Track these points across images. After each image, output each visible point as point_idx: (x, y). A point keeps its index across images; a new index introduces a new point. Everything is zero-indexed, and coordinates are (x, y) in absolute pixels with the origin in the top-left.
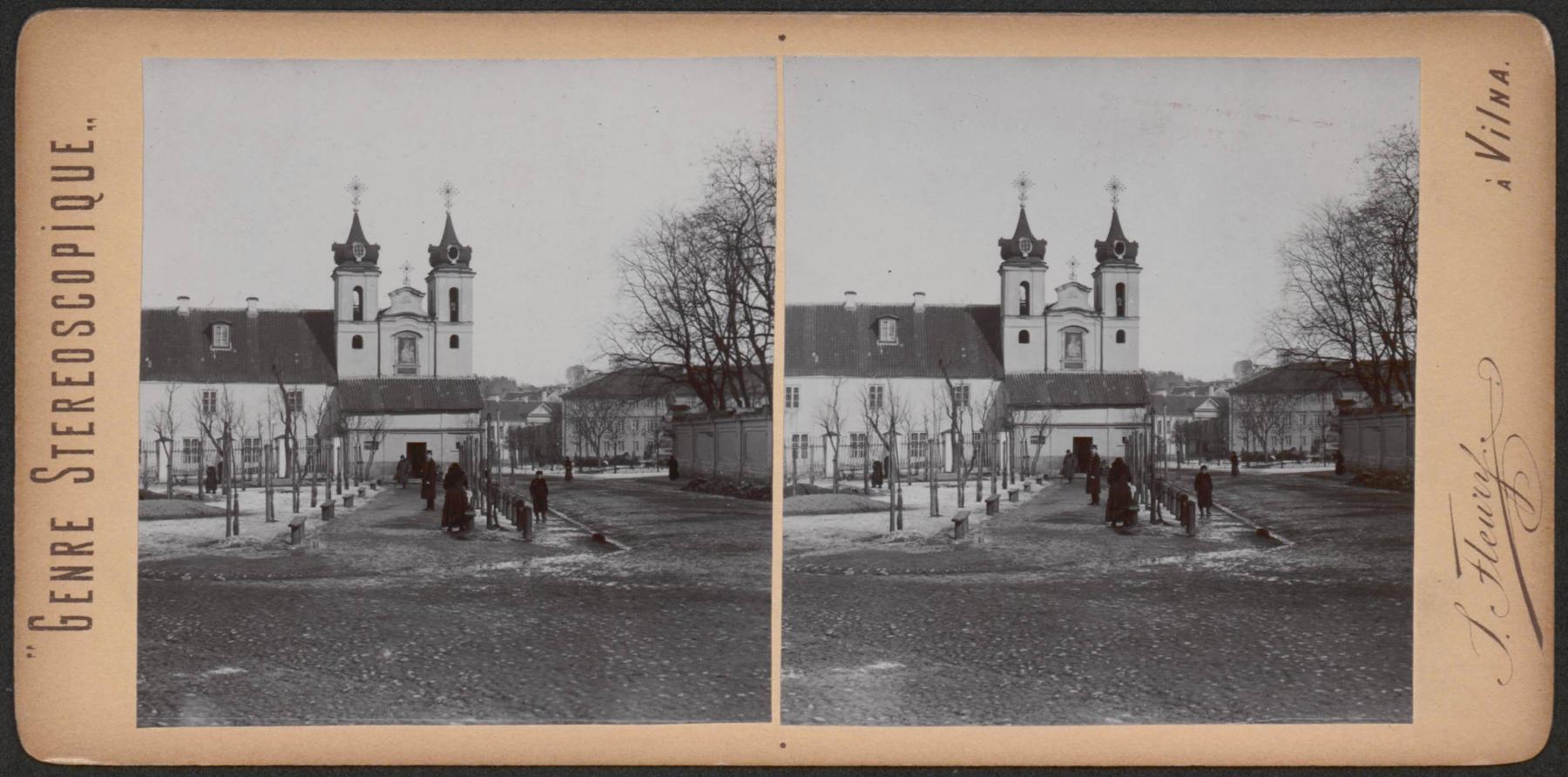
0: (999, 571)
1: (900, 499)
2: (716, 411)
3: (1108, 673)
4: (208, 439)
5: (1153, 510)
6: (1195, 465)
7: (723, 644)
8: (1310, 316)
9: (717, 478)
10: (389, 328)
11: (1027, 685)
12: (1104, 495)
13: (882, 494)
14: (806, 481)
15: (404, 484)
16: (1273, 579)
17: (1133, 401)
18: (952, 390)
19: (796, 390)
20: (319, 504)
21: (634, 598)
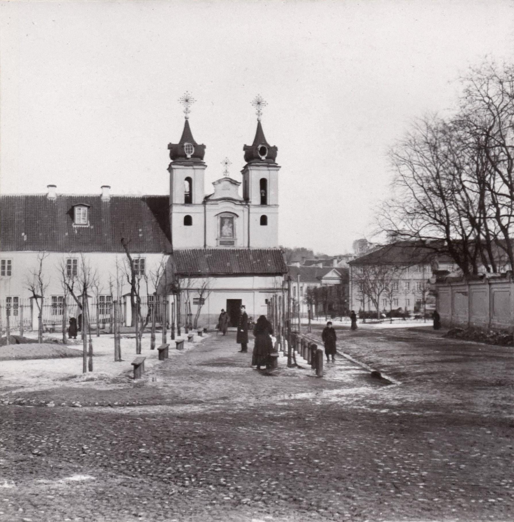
0: (169, 404)
1: (91, 348)
2: (470, 277)
3: (254, 484)
4: (71, 297)
5: (289, 356)
6: (323, 321)
7: (477, 460)
8: (413, 205)
9: (470, 328)
10: (214, 210)
11: (190, 494)
12: (251, 344)
13: (76, 344)
14: (17, 334)
15: (224, 332)
16: (384, 411)
17: (274, 271)
18: (131, 262)
19: (9, 262)
20: (157, 347)
21: (401, 422)
